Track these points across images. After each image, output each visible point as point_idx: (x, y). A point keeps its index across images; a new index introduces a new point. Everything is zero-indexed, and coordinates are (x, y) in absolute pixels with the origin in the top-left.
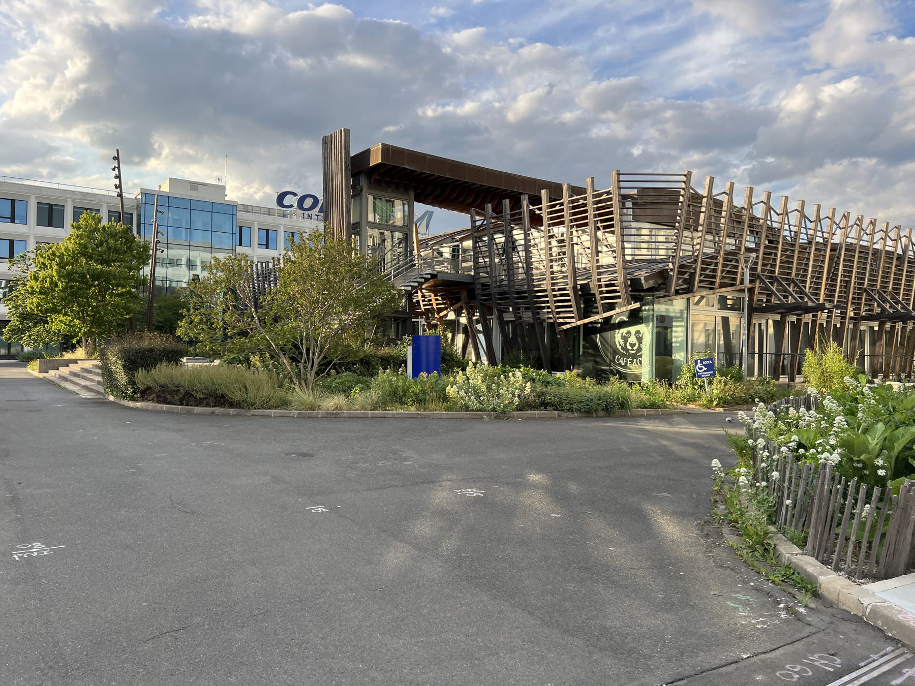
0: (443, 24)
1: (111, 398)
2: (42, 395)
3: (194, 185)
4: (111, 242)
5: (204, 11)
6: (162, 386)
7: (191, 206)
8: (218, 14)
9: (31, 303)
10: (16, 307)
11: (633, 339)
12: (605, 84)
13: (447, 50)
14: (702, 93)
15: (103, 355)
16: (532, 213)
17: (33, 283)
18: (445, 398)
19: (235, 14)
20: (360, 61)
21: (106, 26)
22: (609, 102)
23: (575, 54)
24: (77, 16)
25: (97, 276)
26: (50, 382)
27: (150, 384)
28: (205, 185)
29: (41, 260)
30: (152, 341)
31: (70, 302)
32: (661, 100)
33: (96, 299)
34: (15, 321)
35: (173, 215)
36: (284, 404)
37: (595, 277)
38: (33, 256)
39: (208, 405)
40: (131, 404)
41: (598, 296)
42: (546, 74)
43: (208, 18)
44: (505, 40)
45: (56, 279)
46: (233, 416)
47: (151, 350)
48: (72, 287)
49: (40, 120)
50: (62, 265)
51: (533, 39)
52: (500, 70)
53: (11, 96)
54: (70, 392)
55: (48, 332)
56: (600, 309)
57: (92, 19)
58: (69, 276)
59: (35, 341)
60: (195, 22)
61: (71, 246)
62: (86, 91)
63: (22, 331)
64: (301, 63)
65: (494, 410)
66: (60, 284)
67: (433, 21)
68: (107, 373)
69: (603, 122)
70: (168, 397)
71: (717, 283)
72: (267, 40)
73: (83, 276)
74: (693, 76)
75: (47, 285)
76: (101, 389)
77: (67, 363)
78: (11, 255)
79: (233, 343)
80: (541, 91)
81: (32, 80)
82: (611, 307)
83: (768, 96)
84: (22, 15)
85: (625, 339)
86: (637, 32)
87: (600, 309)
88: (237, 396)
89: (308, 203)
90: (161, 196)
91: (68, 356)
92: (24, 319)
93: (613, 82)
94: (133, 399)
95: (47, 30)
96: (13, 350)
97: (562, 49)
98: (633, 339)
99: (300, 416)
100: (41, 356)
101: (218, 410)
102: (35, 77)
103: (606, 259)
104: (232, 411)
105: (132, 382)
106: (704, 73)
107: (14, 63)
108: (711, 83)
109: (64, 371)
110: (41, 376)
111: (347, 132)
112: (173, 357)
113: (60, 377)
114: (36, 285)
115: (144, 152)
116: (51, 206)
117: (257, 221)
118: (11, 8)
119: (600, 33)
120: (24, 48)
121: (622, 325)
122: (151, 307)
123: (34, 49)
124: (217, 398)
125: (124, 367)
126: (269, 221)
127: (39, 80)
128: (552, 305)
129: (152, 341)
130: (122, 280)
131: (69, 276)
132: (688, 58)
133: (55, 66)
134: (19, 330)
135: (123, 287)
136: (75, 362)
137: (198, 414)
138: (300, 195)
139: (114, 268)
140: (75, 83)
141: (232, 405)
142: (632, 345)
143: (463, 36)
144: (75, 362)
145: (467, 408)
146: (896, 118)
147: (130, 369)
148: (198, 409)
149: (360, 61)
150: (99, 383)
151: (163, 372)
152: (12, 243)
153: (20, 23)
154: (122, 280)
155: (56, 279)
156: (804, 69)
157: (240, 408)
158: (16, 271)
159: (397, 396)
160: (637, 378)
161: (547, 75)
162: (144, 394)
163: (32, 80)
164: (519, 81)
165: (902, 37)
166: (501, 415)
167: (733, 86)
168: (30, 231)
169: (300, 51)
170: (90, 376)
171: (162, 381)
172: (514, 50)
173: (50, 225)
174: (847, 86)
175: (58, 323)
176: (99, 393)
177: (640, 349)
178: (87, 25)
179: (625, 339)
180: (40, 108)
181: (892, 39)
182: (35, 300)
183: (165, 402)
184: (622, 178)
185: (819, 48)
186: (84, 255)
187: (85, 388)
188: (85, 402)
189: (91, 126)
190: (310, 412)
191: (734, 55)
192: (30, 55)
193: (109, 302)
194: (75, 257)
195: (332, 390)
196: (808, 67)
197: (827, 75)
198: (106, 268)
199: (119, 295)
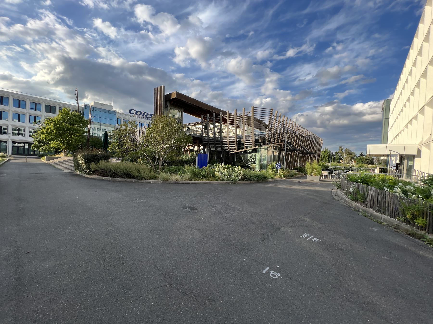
0: (173, 71)
1: (78, 173)
2: (46, 171)
3: (102, 105)
4: (74, 118)
5: (103, 58)
6: (103, 170)
7: (102, 110)
8: (107, 59)
9: (43, 137)
10: (37, 138)
11: (253, 157)
12: (214, 92)
13: (174, 78)
14: (237, 98)
15: (75, 156)
16: (223, 117)
17: (43, 130)
18: (214, 176)
19: (113, 60)
20: (150, 78)
21: (70, 58)
22: (215, 97)
23: (207, 84)
24: (60, 53)
25: (68, 129)
26: (50, 165)
27: (97, 169)
28: (106, 105)
29: (47, 122)
30: (99, 152)
31: (58, 137)
32: (227, 98)
33: (68, 137)
34: (36, 143)
35: (95, 113)
36: (155, 178)
37: (244, 138)
38: (43, 121)
39: (123, 177)
40: (88, 176)
41: (244, 144)
42: (200, 88)
43: (104, 60)
44: (190, 78)
45: (53, 129)
46: (134, 182)
47: (97, 155)
48: (59, 132)
49: (48, 83)
50: (55, 124)
51: (197, 79)
52: (188, 85)
53: (36, 75)
54: (60, 169)
55: (49, 147)
56: (245, 148)
57: (65, 55)
58: (58, 128)
59: (44, 150)
60: (100, 60)
61: (59, 118)
62: (62, 76)
63: (39, 146)
64: (132, 77)
65: (232, 180)
66: (54, 131)
67: (171, 70)
68: (77, 165)
69: (214, 102)
70: (105, 174)
71: (275, 141)
72: (122, 69)
73: (63, 129)
74: (235, 93)
75: (49, 131)
76: (73, 169)
77: (57, 158)
78: (35, 120)
79: (131, 154)
80: (198, 92)
81: (44, 71)
82: (247, 147)
83: (251, 100)
84: (40, 50)
85: (251, 157)
86: (222, 81)
87: (245, 148)
88: (136, 174)
89: (139, 113)
90: (92, 107)
91: (57, 156)
92: (40, 142)
93: (216, 92)
94: (88, 174)
95: (49, 56)
96: (36, 153)
97: (204, 82)
98: (253, 157)
99: (163, 183)
100: (46, 155)
101: (128, 180)
102: (45, 70)
103: (231, 134)
104: (134, 180)
105: (89, 168)
106: (237, 93)
107: (37, 65)
108: (239, 95)
109: (56, 161)
110: (47, 162)
111: (164, 87)
112: (106, 158)
113: (55, 163)
114: (45, 131)
115: (83, 97)
116: (51, 106)
117: (123, 118)
118: (36, 47)
119: (213, 79)
120: (41, 60)
121: (250, 153)
122: (88, 141)
123: (44, 61)
124: (128, 175)
125: (85, 162)
126: (127, 117)
127: (46, 71)
128: (229, 146)
129: (99, 152)
130: (78, 131)
131: (58, 128)
132: (234, 88)
133: (51, 68)
134: (38, 146)
135: (79, 133)
136: (60, 158)
137: (119, 181)
138: (136, 111)
139: (76, 127)
140: (59, 73)
141: (134, 178)
142: (253, 159)
143: (179, 75)
144: (60, 158)
145: (223, 180)
146: (278, 108)
147: (88, 162)
148: (119, 179)
149: (150, 78)
150: (71, 166)
151: (102, 164)
152: (35, 117)
153: (39, 52)
154: (78, 131)
155: (53, 129)
156: (259, 95)
157: (137, 179)
158: (36, 126)
159: (195, 175)
160: (254, 168)
161: (200, 88)
162: (94, 172)
163: (44, 71)
164: (193, 89)
165: (280, 90)
166: (234, 182)
167: (244, 97)
168: (43, 114)
169: (132, 73)
170: (67, 163)
171: (102, 168)
172: (192, 81)
173: (50, 112)
174: (268, 100)
175: (53, 144)
176: (72, 170)
177: (255, 160)
178: (63, 56)
179: (251, 157)
180: (46, 80)
181: (278, 90)
182: (44, 136)
183: (104, 176)
184: (255, 108)
185: (263, 90)
186: (64, 122)
187: (66, 168)
188: (66, 174)
189: (65, 87)
190: (166, 181)
191: (244, 89)
192: (42, 63)
193: (74, 138)
194: (60, 122)
195: (175, 172)
196: (260, 94)
197: (264, 96)
198: (72, 127)
199: (77, 136)
